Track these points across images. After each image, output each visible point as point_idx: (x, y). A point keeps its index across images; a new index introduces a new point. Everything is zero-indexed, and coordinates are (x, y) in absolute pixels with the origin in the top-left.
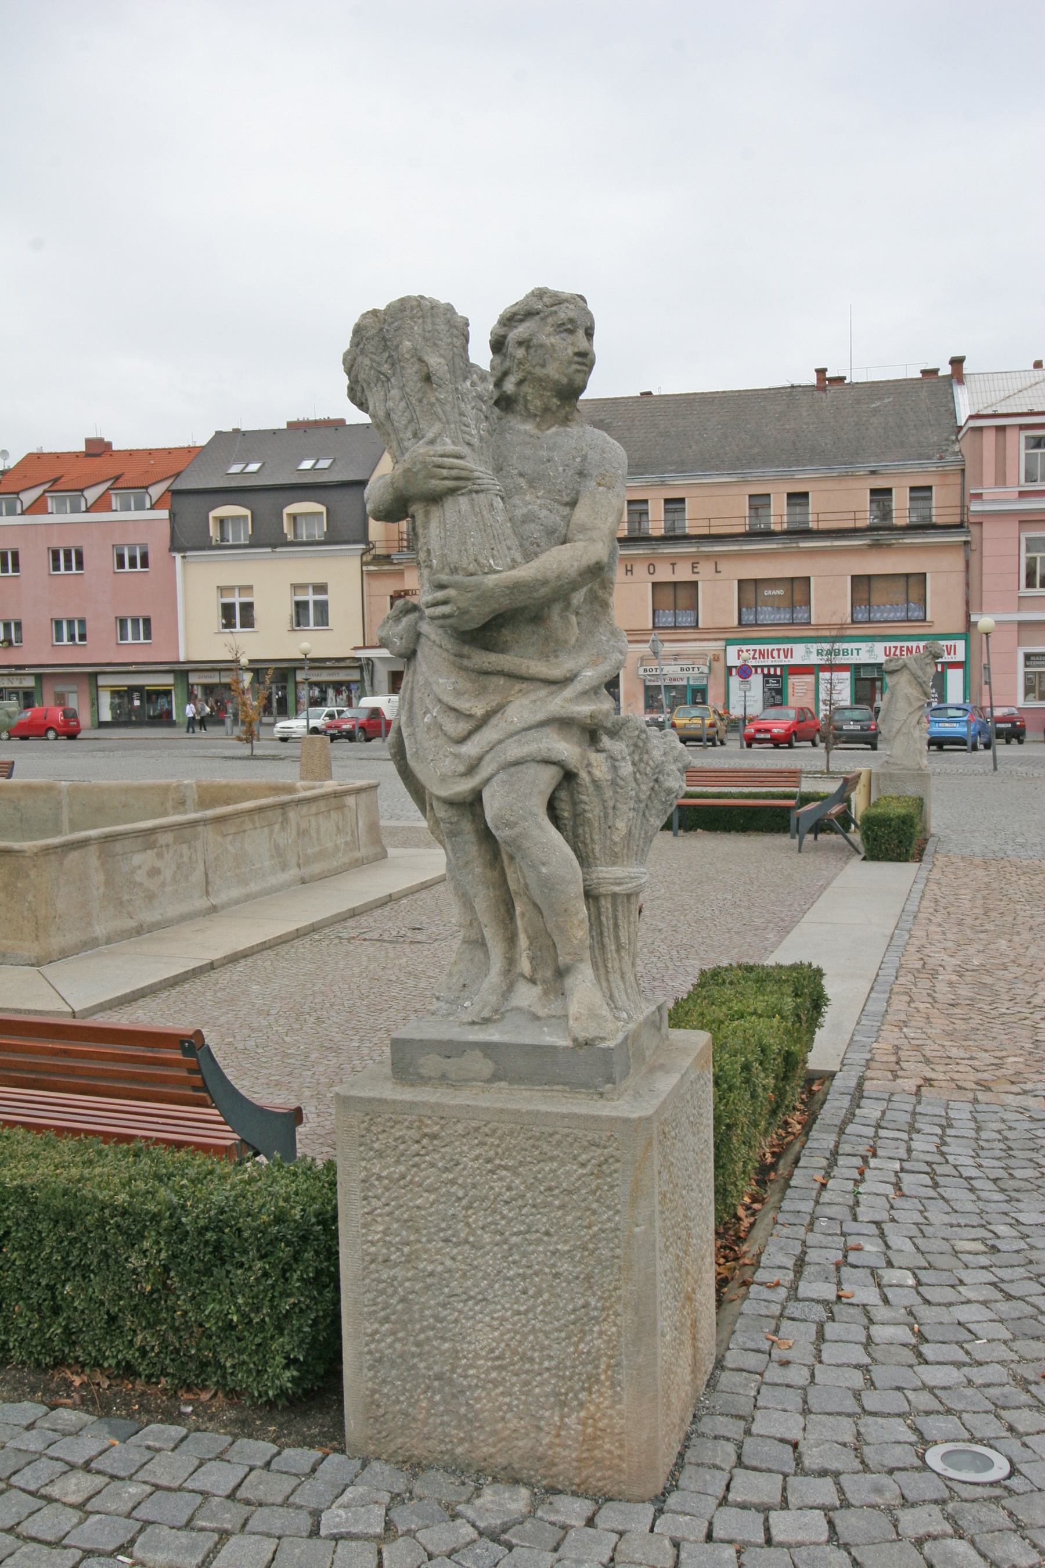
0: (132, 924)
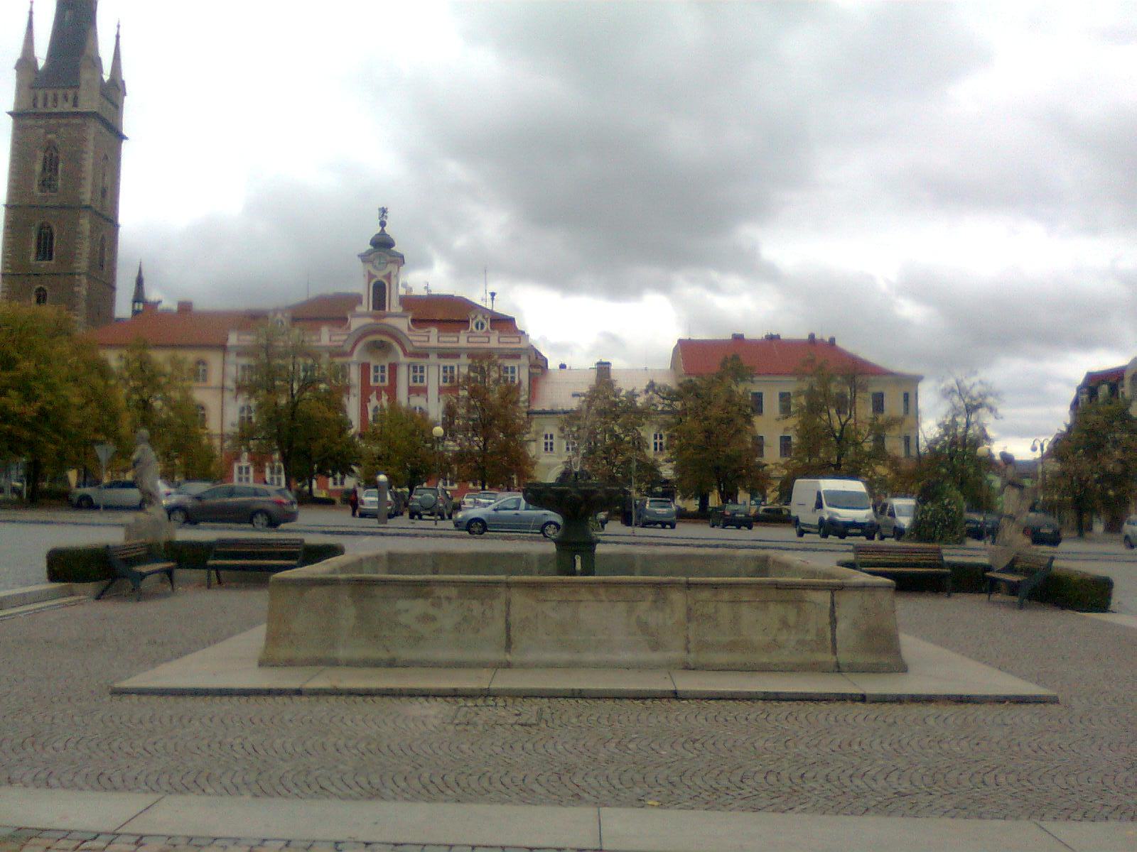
0: (383, 655)
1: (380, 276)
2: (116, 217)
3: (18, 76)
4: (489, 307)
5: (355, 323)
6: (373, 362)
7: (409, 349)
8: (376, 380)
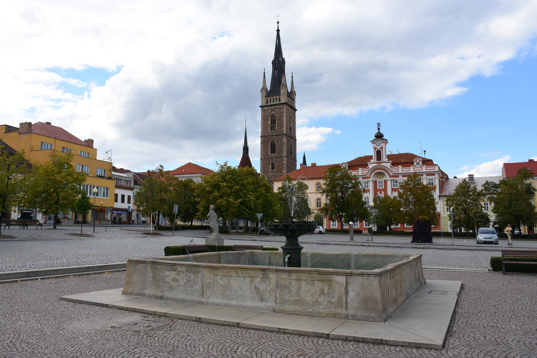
0: (160, 294)
6: (378, 180)
7: (391, 174)
8: (379, 187)
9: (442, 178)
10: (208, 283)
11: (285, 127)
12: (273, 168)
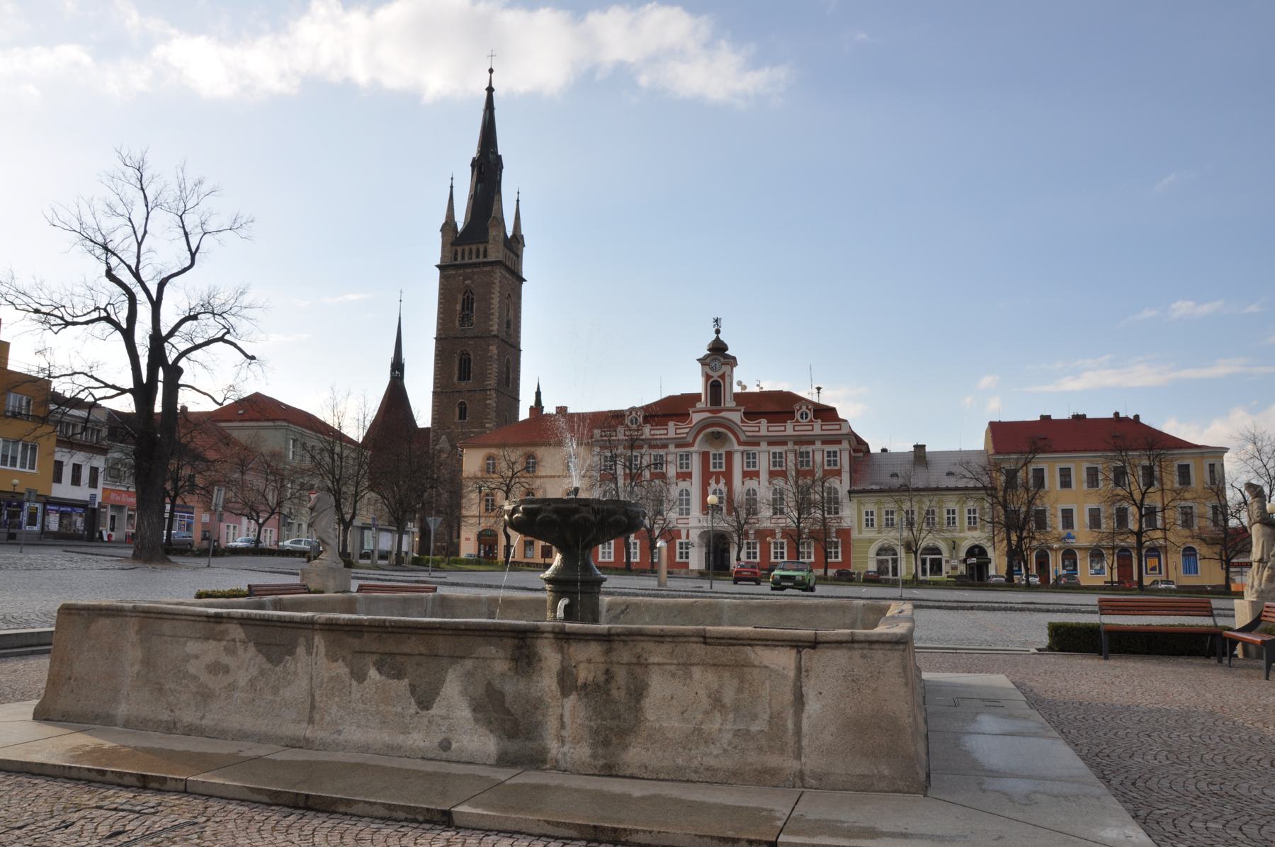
0: (165, 716)
1: (715, 375)
2: (519, 343)
3: (443, 237)
4: (815, 400)
5: (696, 418)
6: (712, 451)
7: (743, 438)
9: (855, 451)
10: (331, 679)
11: (495, 320)
12: (463, 415)
